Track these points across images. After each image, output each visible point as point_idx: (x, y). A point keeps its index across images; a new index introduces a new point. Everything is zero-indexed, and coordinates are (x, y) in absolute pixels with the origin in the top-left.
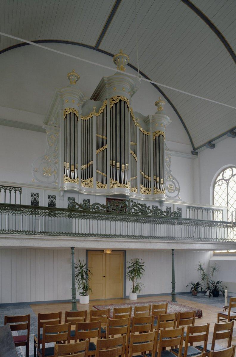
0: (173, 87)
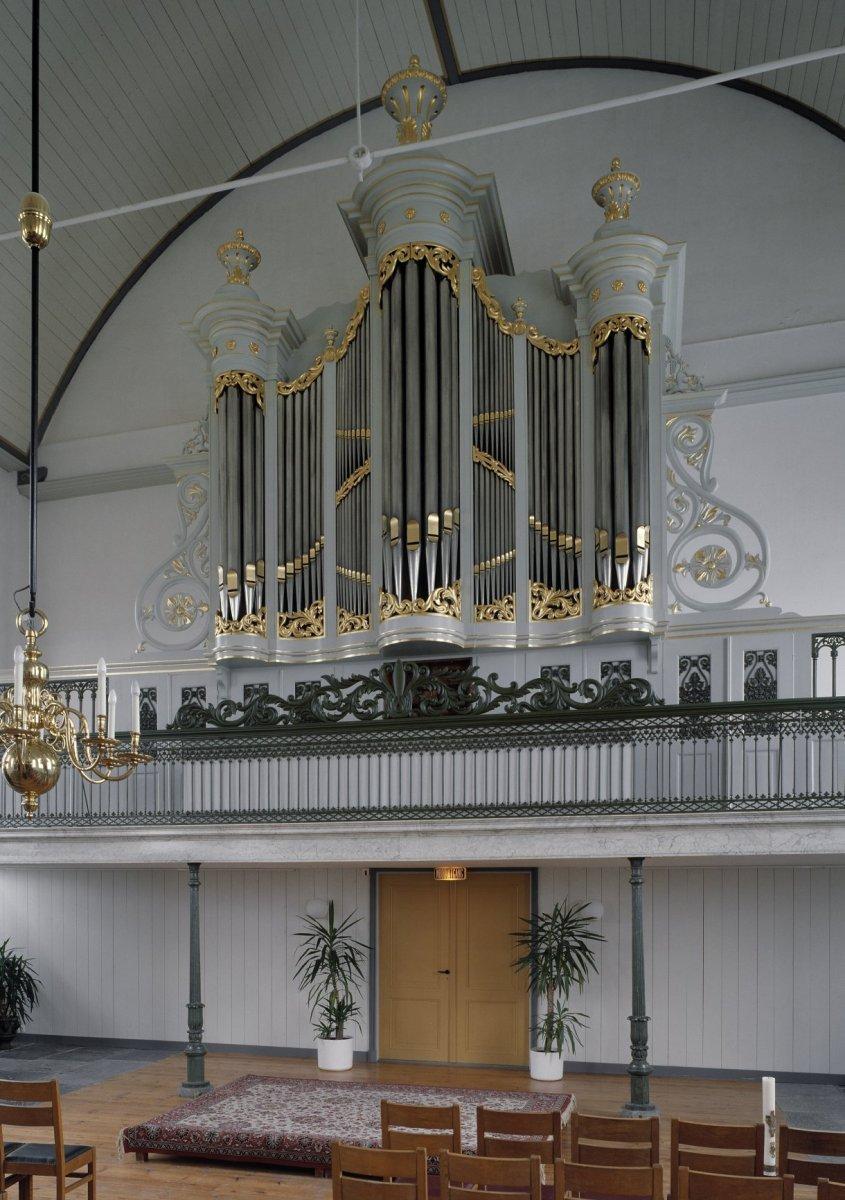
0: (810, 50)
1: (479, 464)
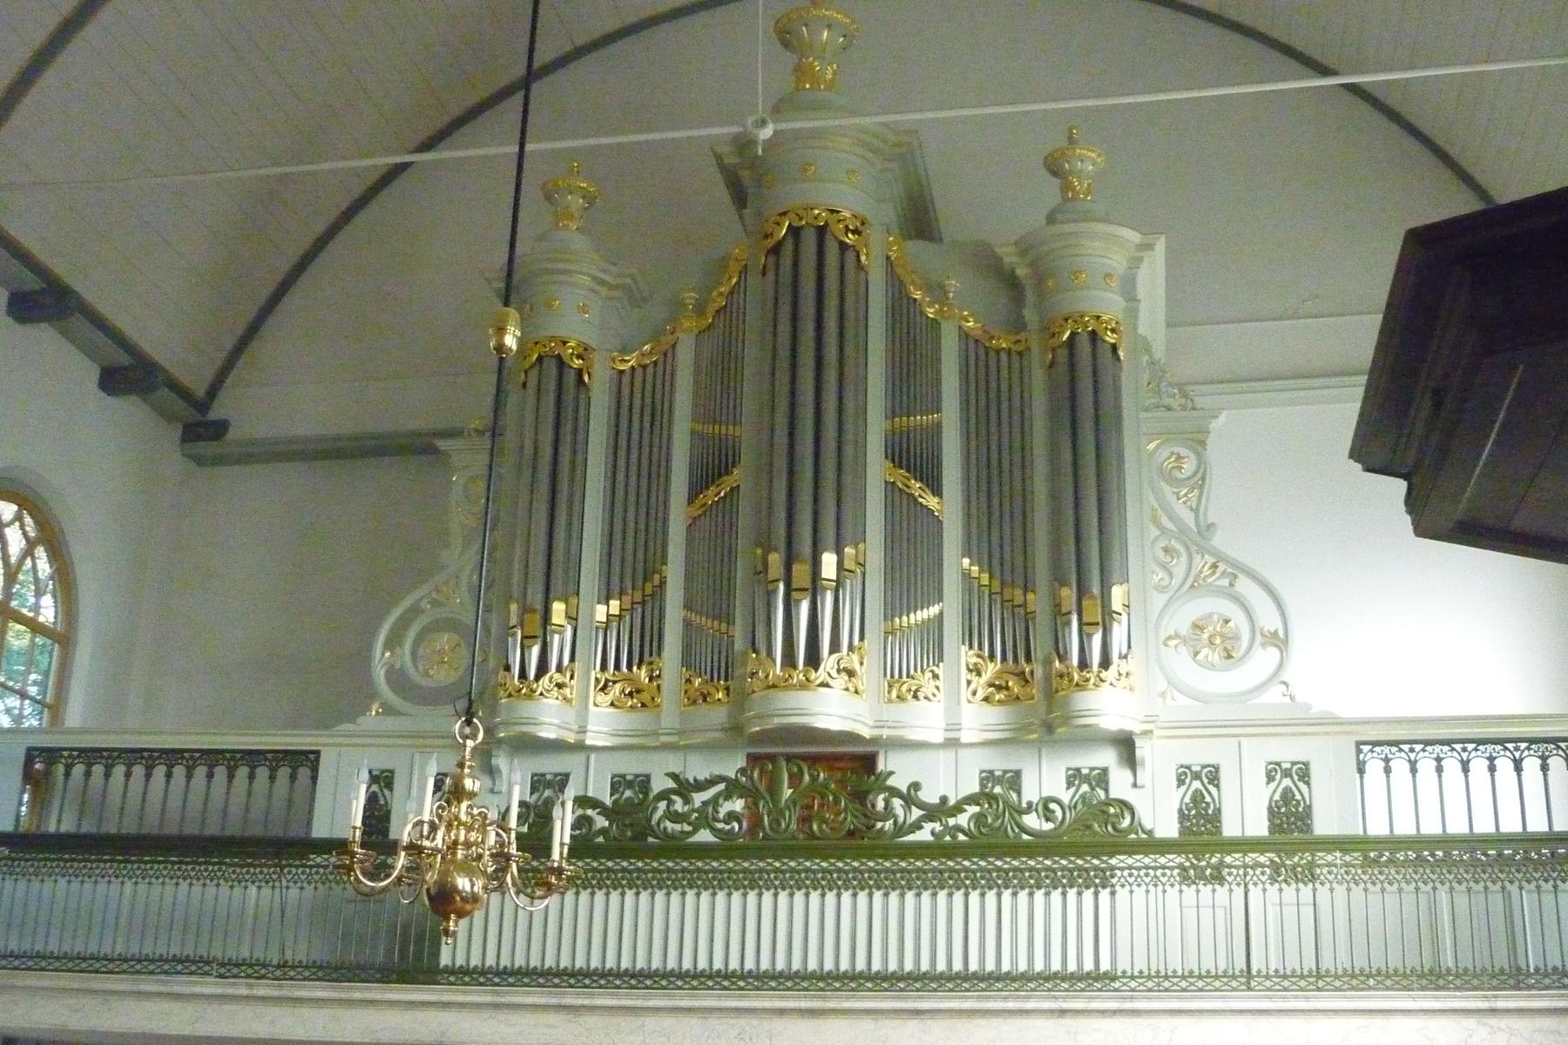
1: (893, 483)
